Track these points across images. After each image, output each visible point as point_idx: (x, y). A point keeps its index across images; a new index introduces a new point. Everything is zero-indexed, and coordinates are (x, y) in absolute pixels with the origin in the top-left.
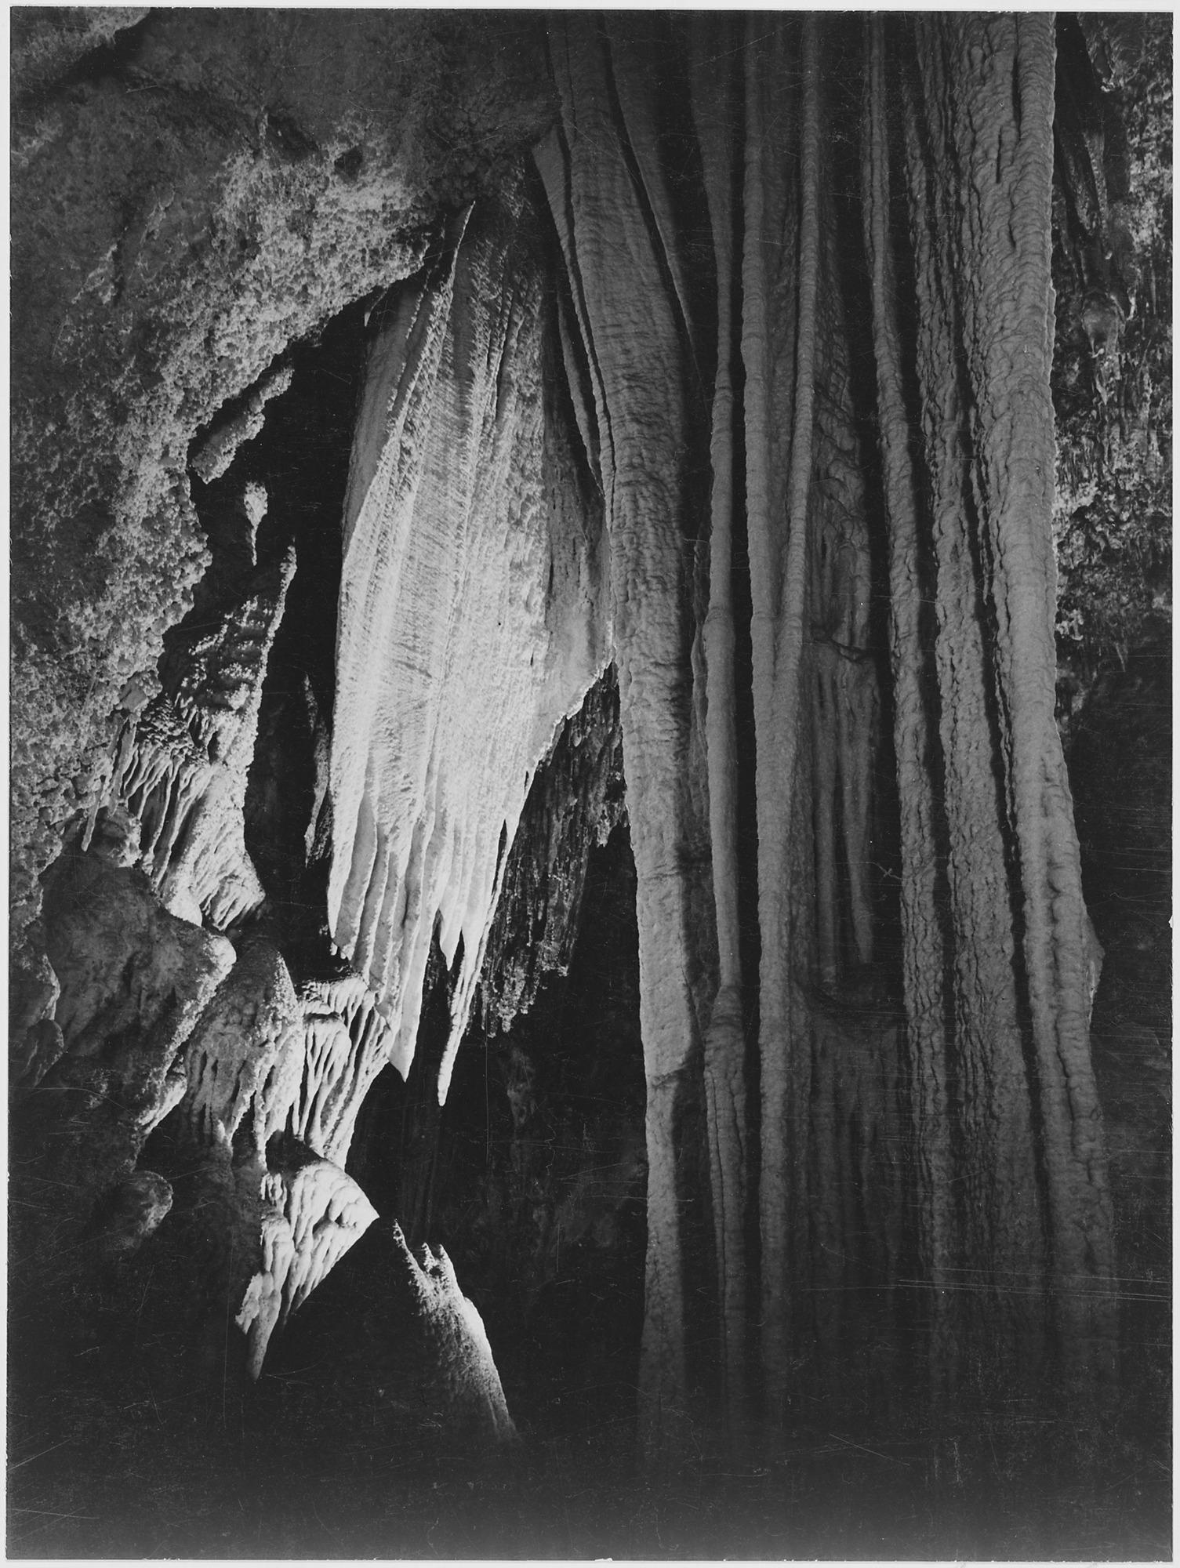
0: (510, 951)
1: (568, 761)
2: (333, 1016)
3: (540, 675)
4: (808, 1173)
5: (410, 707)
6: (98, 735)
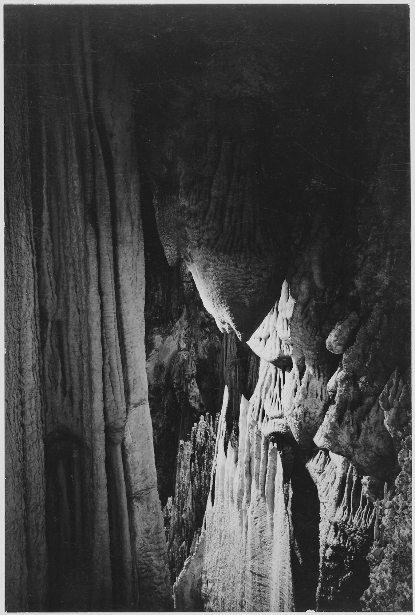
0: (204, 448)
1: (187, 534)
2: (273, 418)
3: (203, 576)
4: (83, 371)
5: (258, 556)
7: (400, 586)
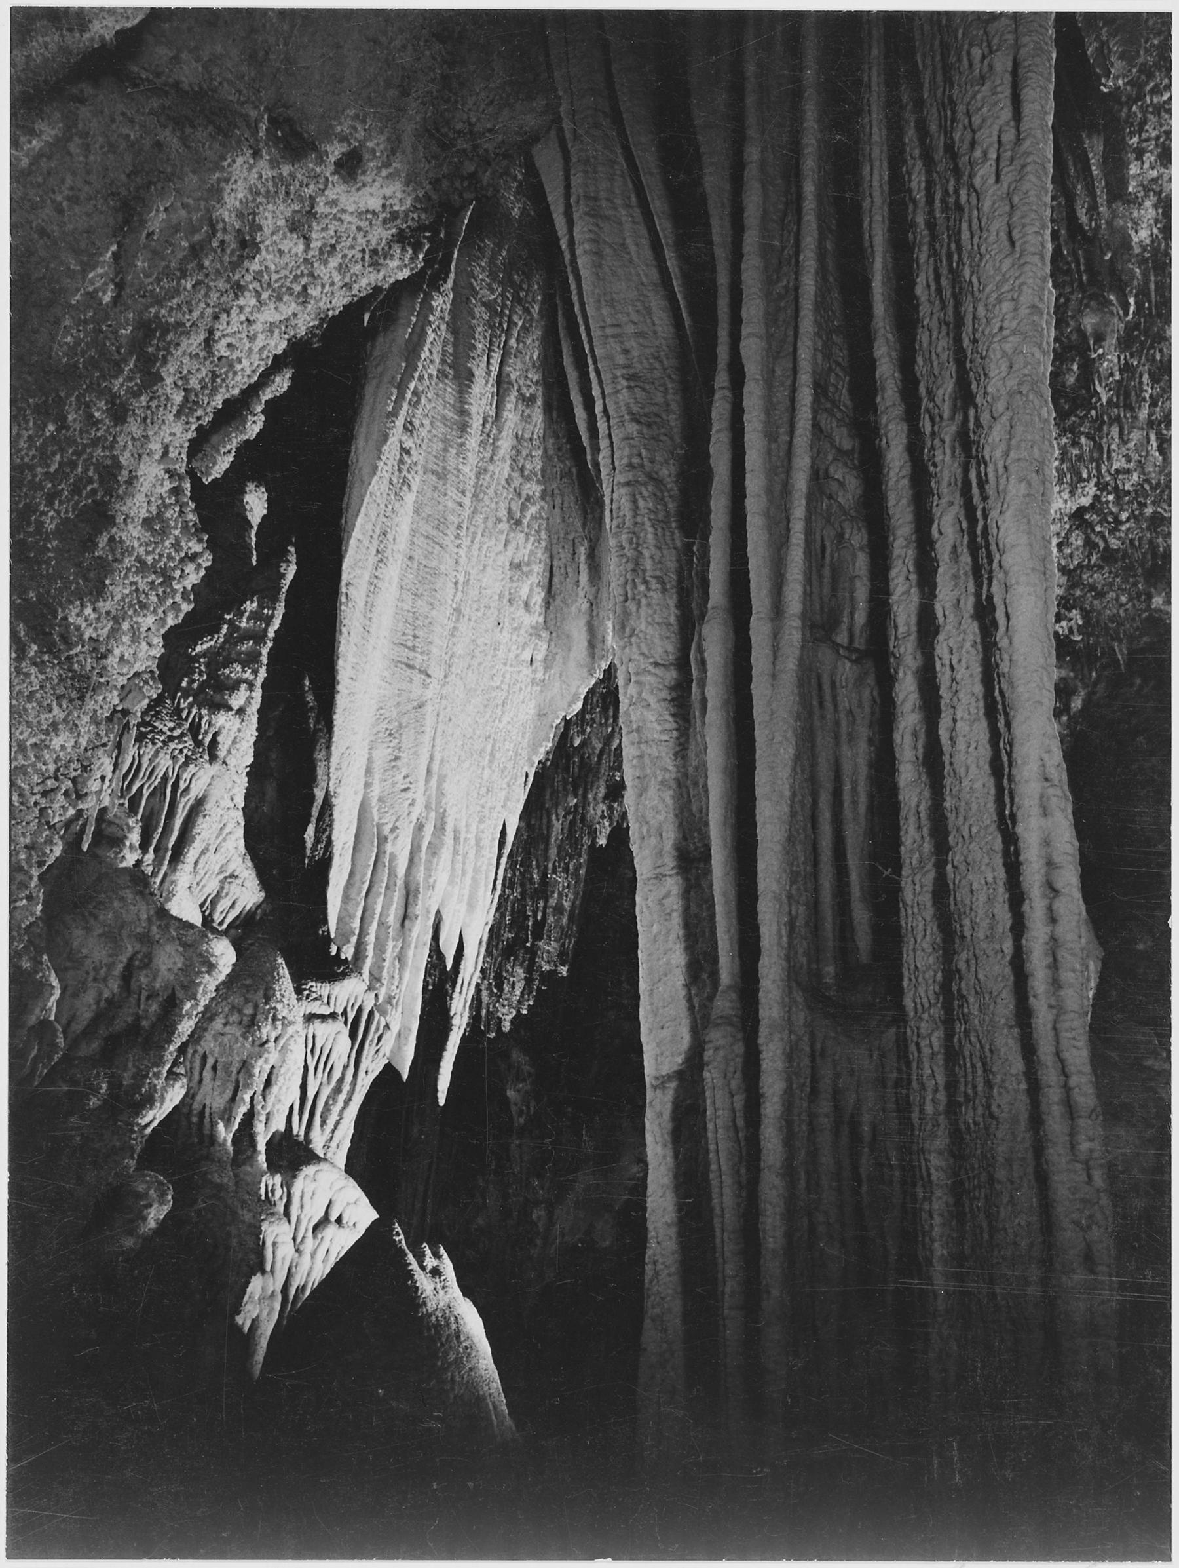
0: (509, 951)
2: (333, 1016)
3: (540, 675)
5: (410, 707)
6: (98, 735)
7: (100, 632)
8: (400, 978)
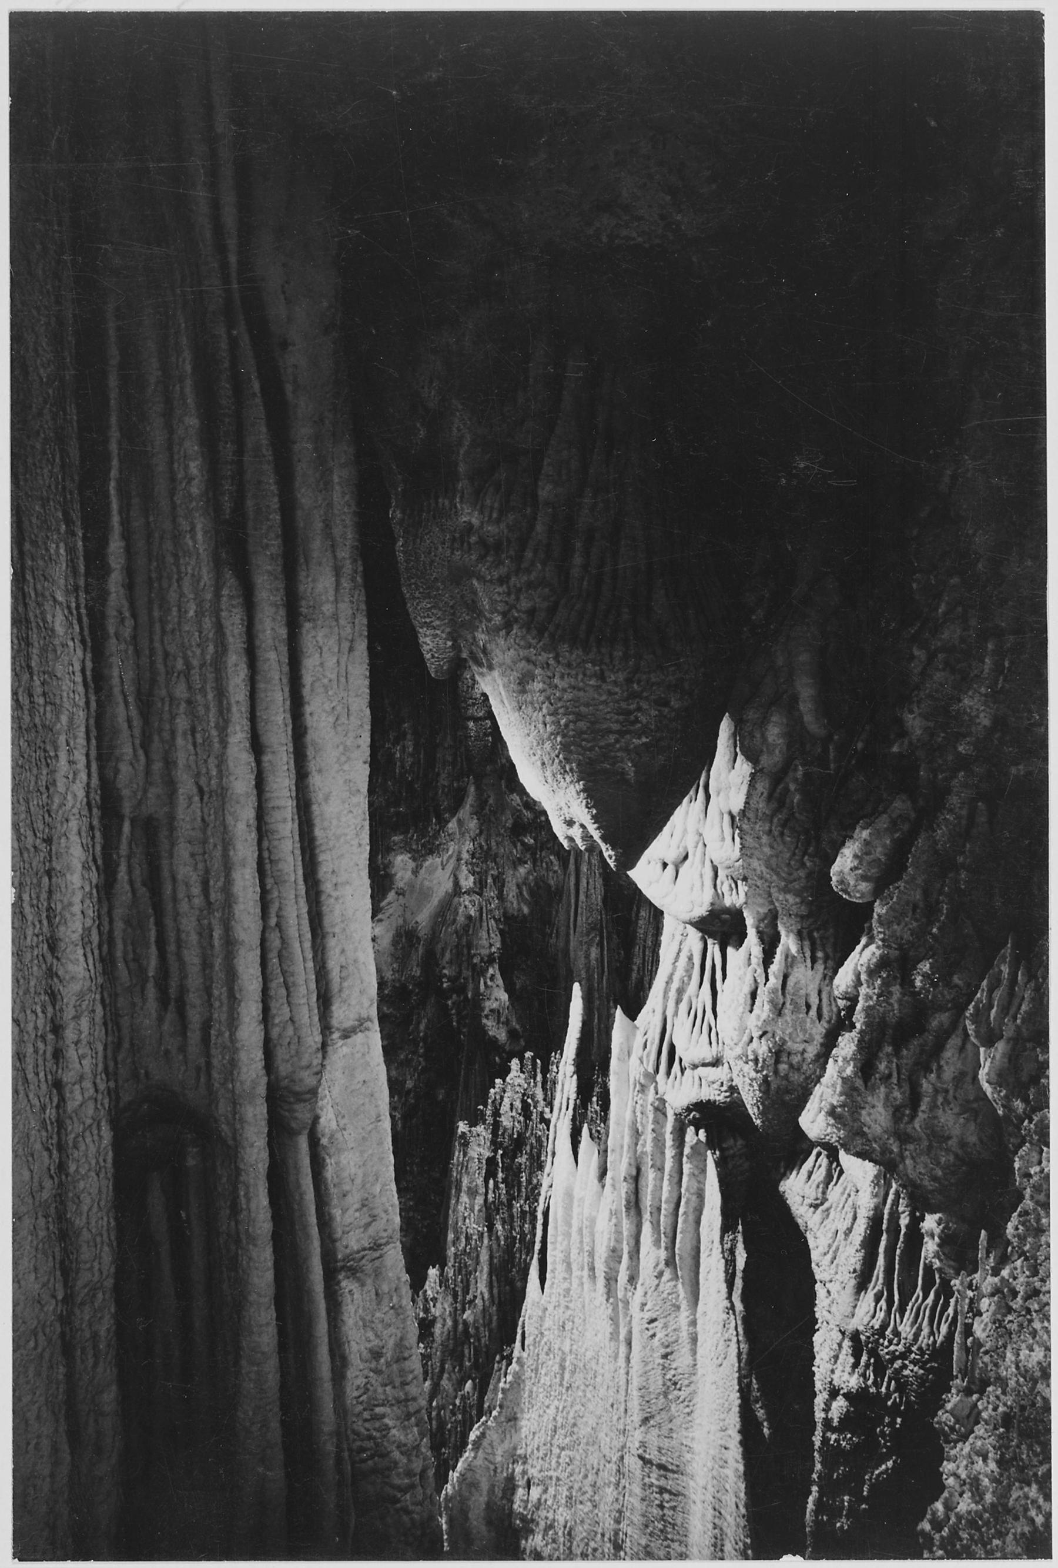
0: (519, 1143)
1: (476, 1360)
2: (695, 1067)
3: (519, 1469)
4: (212, 946)
5: (658, 1418)
6: (996, 1365)
7: (1021, 1493)
8: (634, 1112)
